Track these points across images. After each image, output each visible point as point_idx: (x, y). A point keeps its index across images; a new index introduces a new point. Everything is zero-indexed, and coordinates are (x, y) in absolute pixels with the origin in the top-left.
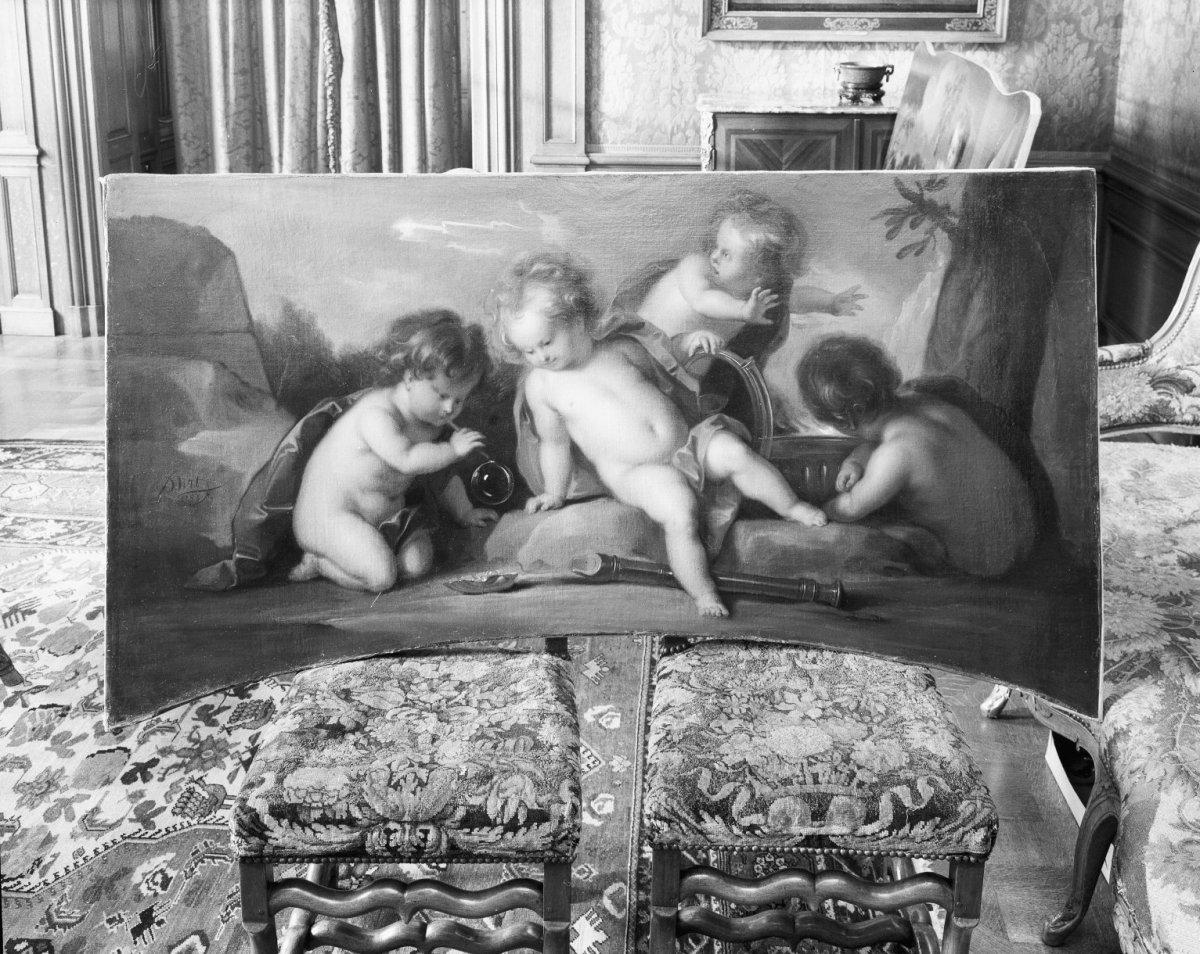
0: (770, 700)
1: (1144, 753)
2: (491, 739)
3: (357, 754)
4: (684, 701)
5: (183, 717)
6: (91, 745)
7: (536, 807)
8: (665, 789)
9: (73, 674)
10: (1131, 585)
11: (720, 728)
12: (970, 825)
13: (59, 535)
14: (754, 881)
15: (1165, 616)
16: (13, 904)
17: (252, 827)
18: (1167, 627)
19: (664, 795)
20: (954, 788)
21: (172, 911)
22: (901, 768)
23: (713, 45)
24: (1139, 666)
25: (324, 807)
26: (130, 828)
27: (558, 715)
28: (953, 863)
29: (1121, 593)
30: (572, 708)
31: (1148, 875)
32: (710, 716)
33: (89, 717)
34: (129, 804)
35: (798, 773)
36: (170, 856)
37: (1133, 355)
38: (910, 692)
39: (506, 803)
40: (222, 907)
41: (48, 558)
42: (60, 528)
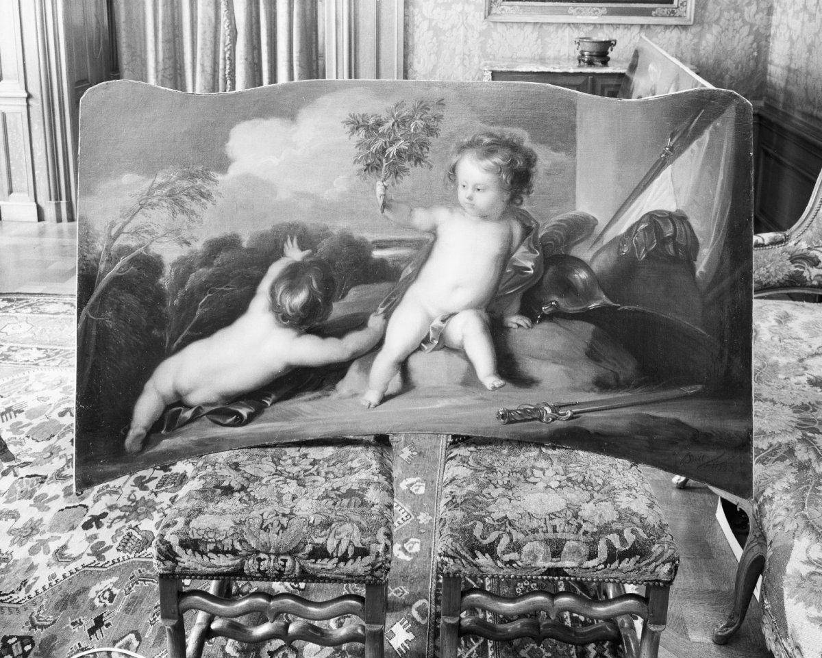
0: (524, 474)
1: (784, 513)
2: (332, 498)
3: (241, 506)
4: (465, 475)
5: (126, 484)
6: (62, 503)
7: (360, 546)
8: (451, 536)
9: (49, 454)
10: (775, 398)
11: (489, 494)
12: (661, 560)
13: (39, 359)
14: (513, 598)
15: (798, 418)
16: (7, 611)
17: (168, 554)
18: (800, 426)
19: (450, 540)
20: (649, 535)
21: (116, 617)
22: (613, 522)
23: (492, 25)
24: (780, 453)
25: (216, 542)
26: (88, 560)
27: (379, 483)
28: (648, 587)
29: (768, 403)
30: (390, 479)
31: (785, 596)
32: (482, 486)
33: (59, 483)
34: (87, 544)
35: (543, 525)
36: (115, 579)
37: (778, 240)
38: (620, 470)
39: (340, 542)
40: (150, 614)
41: (32, 374)
42: (40, 354)
